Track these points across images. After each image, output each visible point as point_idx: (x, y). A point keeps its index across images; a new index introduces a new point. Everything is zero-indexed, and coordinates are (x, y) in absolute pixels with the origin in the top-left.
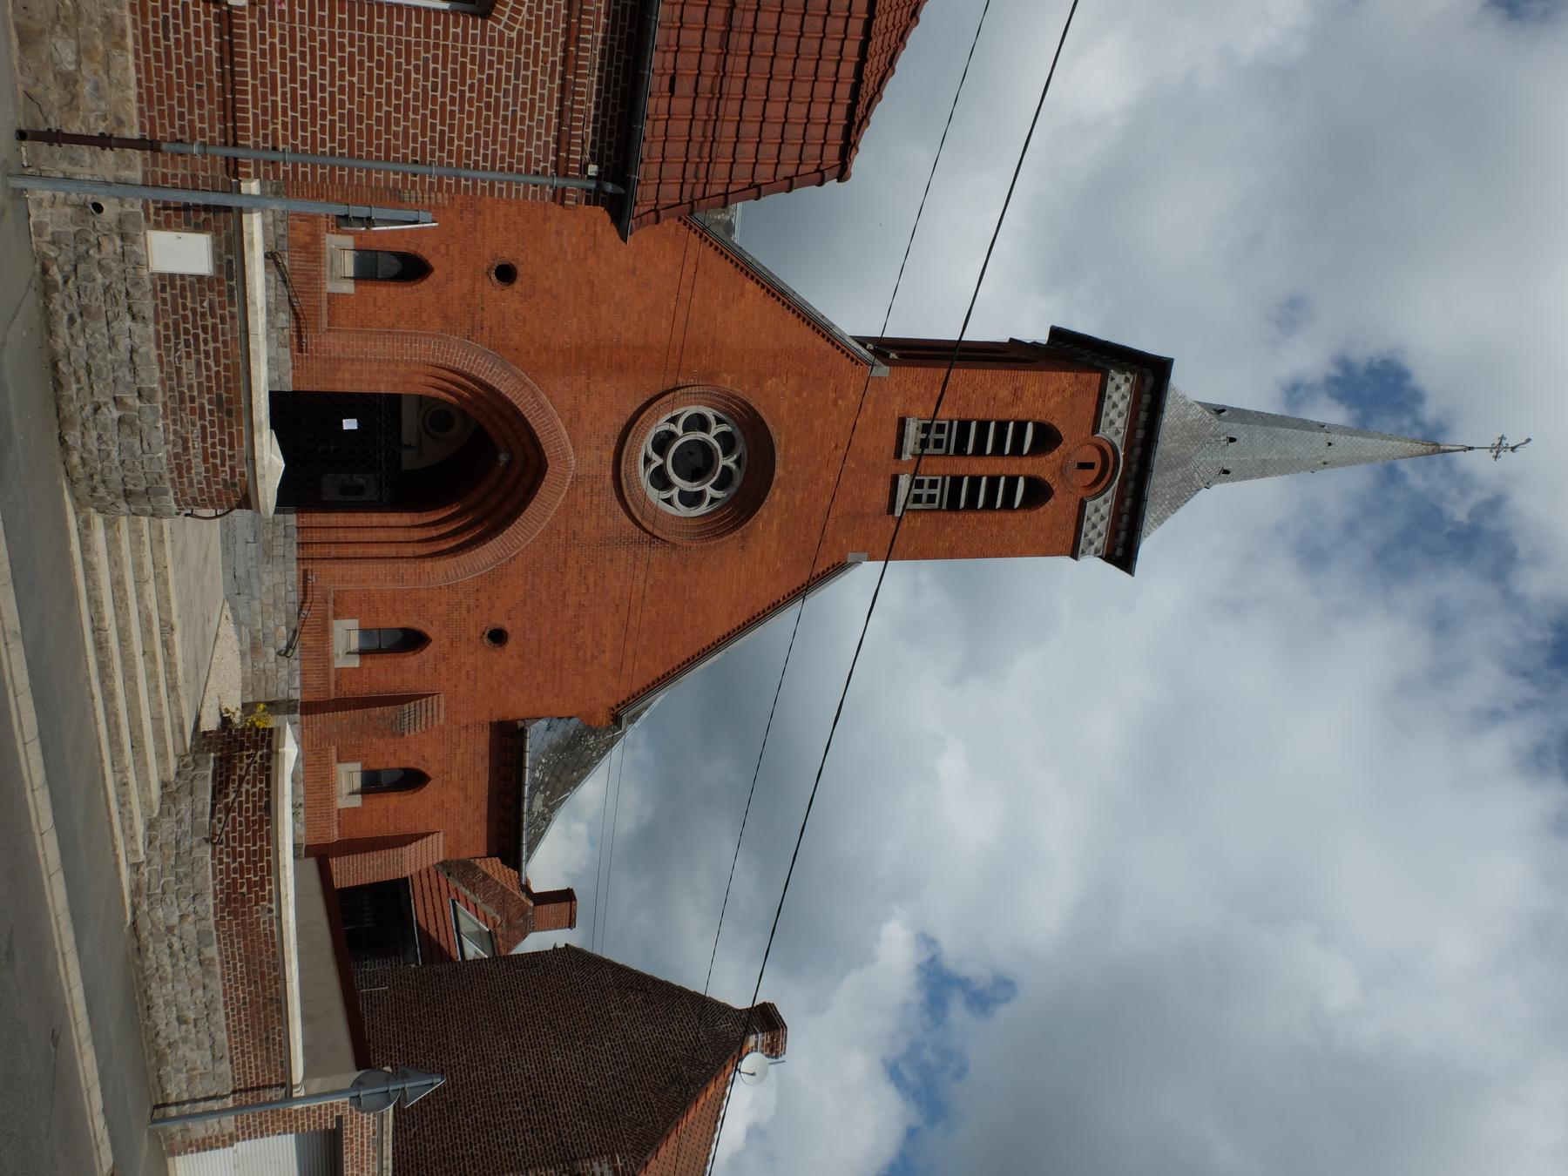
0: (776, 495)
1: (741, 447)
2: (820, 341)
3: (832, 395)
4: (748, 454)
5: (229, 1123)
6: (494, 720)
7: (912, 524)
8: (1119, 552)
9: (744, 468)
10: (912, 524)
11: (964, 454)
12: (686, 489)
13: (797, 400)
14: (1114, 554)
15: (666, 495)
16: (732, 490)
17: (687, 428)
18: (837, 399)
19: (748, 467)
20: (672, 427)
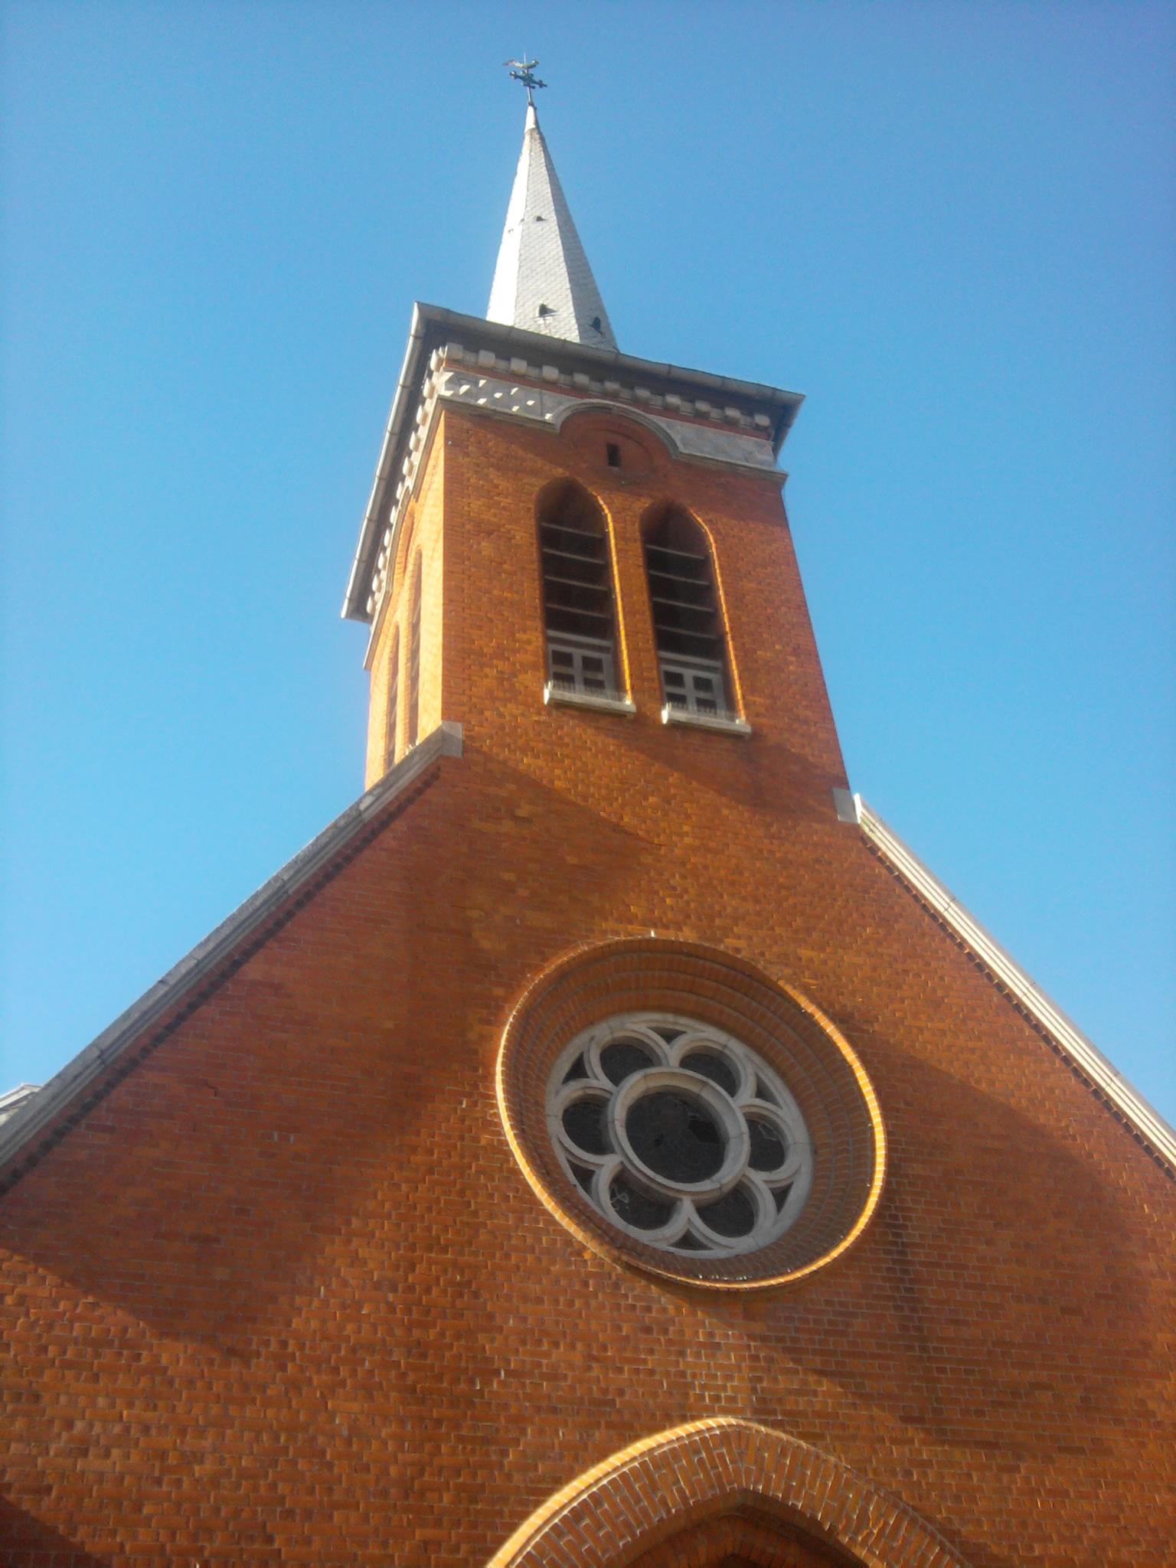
0: (736, 944)
1: (639, 1026)
2: (387, 839)
3: (507, 826)
4: (661, 1009)
5: (362, 807)
6: (591, 323)
7: (763, 710)
8: (763, 420)
9: (683, 1022)
10: (763, 710)
11: (658, 664)
12: (746, 1148)
13: (522, 892)
14: (765, 429)
15: (766, 1202)
16: (737, 1051)
17: (599, 1145)
18: (515, 818)
19: (678, 1011)
20: (701, 1229)
